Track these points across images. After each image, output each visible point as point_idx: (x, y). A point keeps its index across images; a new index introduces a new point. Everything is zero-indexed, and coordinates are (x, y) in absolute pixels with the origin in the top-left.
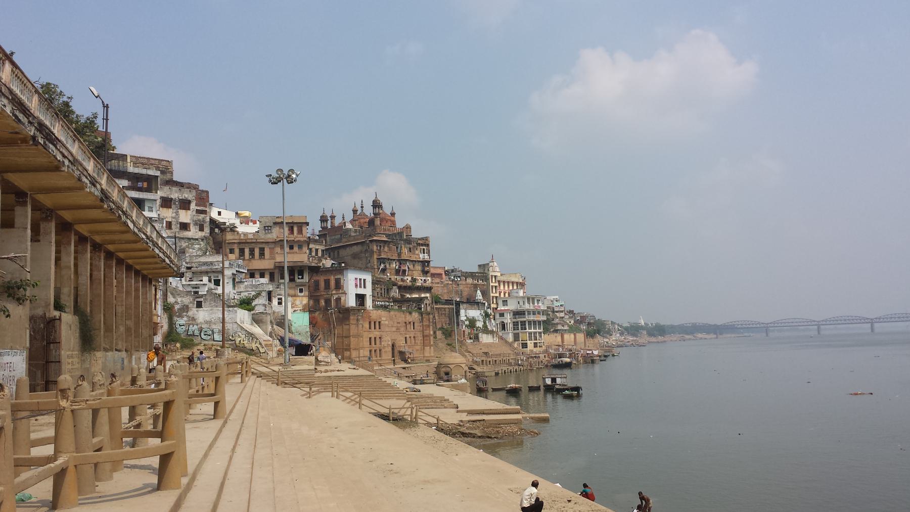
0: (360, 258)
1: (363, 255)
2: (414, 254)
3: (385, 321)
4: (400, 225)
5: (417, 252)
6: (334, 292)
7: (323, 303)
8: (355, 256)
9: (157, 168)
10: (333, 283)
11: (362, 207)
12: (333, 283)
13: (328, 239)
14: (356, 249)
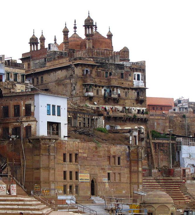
0: (65, 85)
1: (68, 81)
2: (127, 80)
4: (117, 47)
5: (130, 78)
6: (24, 119)
8: (59, 82)
11: (75, 28)
13: (32, 63)
14: (61, 74)
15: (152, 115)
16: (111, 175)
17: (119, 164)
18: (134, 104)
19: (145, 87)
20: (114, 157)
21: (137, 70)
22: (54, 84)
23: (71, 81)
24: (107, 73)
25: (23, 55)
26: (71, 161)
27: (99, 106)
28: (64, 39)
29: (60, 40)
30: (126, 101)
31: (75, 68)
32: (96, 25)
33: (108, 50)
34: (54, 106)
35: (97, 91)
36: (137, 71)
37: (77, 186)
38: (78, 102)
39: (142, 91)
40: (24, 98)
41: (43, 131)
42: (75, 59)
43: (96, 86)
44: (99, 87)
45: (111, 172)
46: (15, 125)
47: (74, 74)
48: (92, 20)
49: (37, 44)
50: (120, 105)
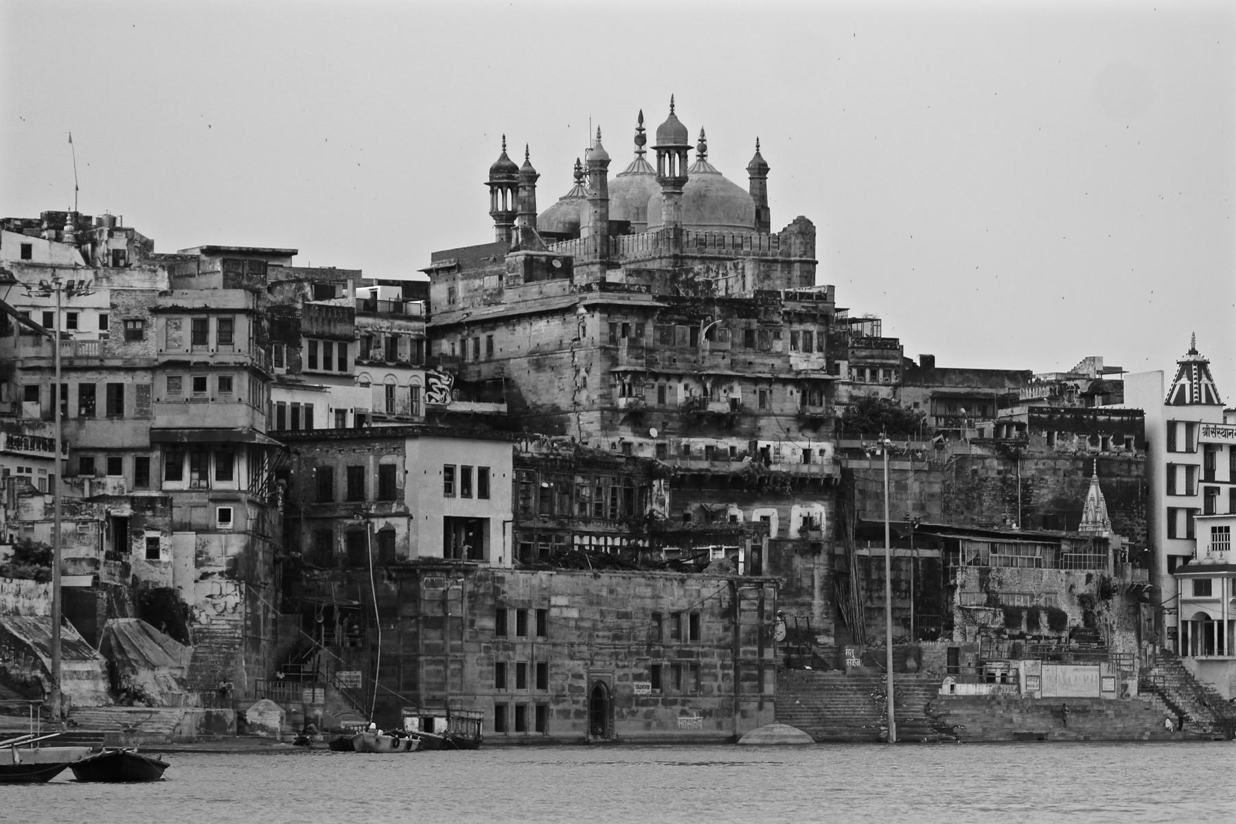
2: (768, 352)
3: (563, 607)
5: (778, 346)
7: (341, 544)
14: (547, 331)
20: (676, 615)
22: (524, 362)
27: (666, 442)
36: (801, 322)
40: (378, 446)
41: (427, 542)
43: (656, 376)
44: (668, 377)
50: (738, 435)
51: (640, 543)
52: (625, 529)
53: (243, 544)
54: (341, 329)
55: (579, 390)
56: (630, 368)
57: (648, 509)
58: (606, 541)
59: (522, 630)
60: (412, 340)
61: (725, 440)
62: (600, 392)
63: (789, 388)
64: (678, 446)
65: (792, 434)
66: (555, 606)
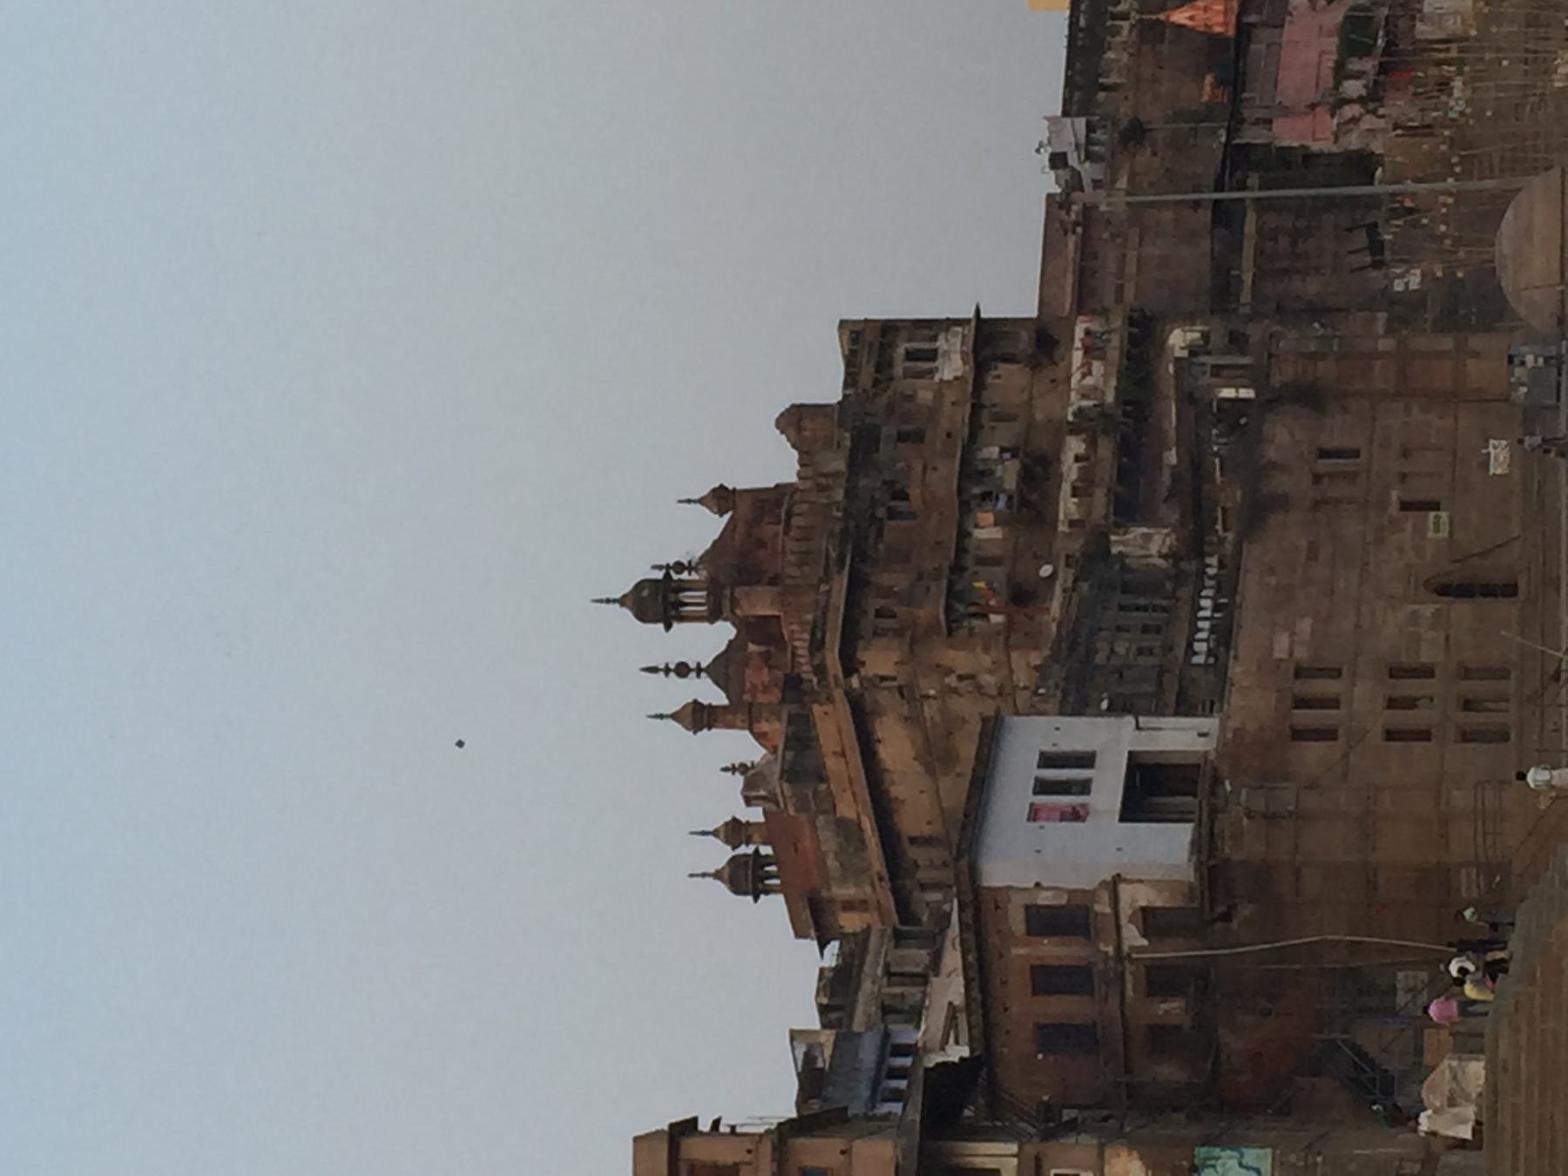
1: (930, 710)
2: (933, 412)
3: (1289, 643)
4: (777, 465)
5: (925, 396)
7: (1171, 1009)
8: (935, 757)
9: (1388, 44)
10: (1052, 950)
11: (682, 670)
12: (1052, 950)
15: (1120, 290)
16: (1408, 498)
17: (1356, 454)
18: (1053, 381)
19: (968, 321)
20: (1317, 478)
21: (884, 365)
22: (946, 783)
23: (932, 692)
24: (893, 514)
25: (799, 934)
26: (1333, 703)
28: (731, 726)
29: (742, 746)
30: (1039, 416)
31: (863, 671)
32: (668, 567)
33: (791, 506)
34: (1043, 787)
35: (981, 561)
36: (891, 365)
37: (1466, 673)
38: (1036, 659)
39: (988, 337)
40: (993, 940)
42: (820, 670)
43: (957, 568)
44: (961, 550)
45: (1394, 495)
46: (1134, 991)
47: (894, 679)
48: (640, 586)
49: (758, 860)
51: (1211, 571)
52: (1185, 593)
53: (1124, 1153)
54: (868, 1053)
55: (979, 688)
56: (942, 602)
57: (1161, 562)
58: (1205, 619)
59: (1333, 703)
60: (896, 947)
61: (1064, 469)
62: (979, 650)
63: (989, 380)
64: (1067, 535)
65: (1060, 374)
66: (1291, 654)
